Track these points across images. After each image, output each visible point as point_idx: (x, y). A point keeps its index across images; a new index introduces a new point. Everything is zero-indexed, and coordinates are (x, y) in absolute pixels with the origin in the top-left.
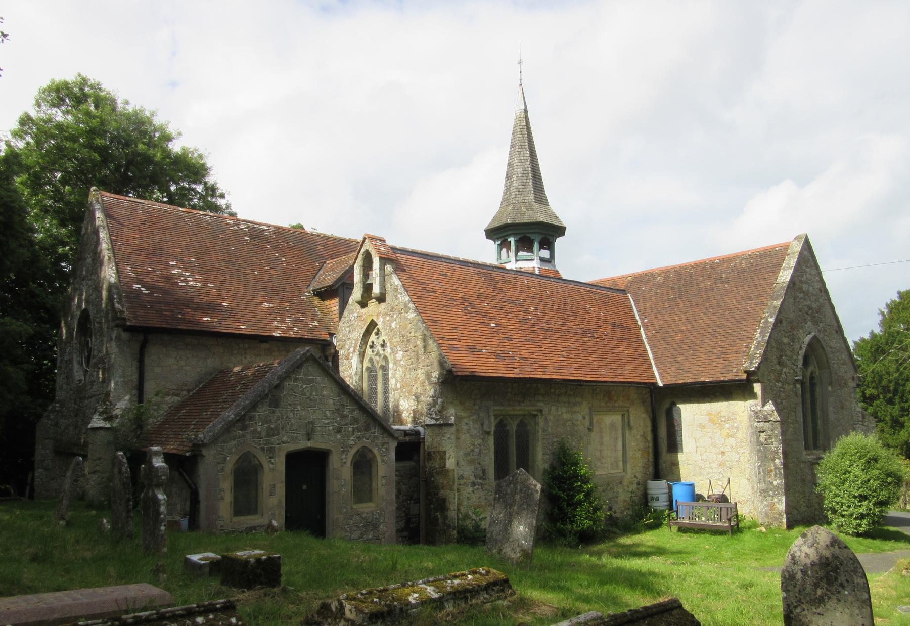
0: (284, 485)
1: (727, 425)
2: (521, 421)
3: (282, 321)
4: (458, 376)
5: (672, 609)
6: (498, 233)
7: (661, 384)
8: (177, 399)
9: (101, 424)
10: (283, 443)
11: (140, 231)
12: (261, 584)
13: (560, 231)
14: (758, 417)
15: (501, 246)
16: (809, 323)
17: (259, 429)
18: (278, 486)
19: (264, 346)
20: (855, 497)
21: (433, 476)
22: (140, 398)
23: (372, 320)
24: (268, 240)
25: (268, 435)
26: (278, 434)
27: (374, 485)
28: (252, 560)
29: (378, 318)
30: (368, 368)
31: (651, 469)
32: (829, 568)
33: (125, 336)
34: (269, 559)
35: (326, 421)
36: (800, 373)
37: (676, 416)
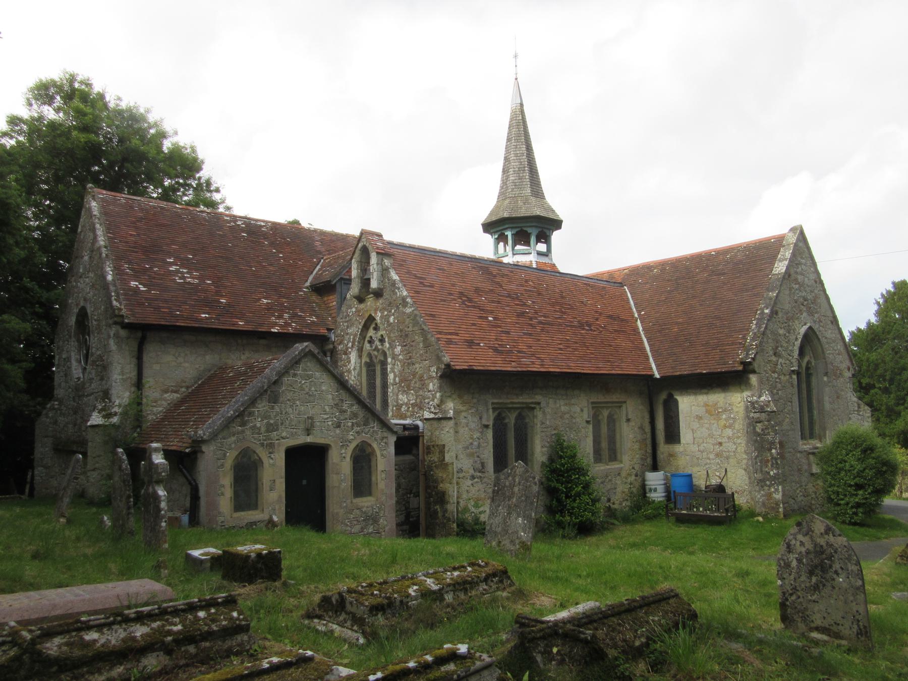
0: (284, 480)
1: (724, 416)
3: (280, 317)
4: (456, 370)
8: (176, 395)
10: (283, 438)
12: (262, 578)
13: (557, 224)
14: (754, 408)
15: (498, 241)
16: (805, 314)
17: (258, 425)
18: (277, 481)
19: (263, 342)
20: (851, 486)
23: (370, 315)
24: (265, 236)
25: (268, 431)
26: (277, 430)
27: (373, 479)
28: (253, 555)
30: (366, 363)
31: (649, 460)
32: (824, 556)
33: (123, 333)
34: (270, 553)
35: (326, 416)
36: (796, 364)
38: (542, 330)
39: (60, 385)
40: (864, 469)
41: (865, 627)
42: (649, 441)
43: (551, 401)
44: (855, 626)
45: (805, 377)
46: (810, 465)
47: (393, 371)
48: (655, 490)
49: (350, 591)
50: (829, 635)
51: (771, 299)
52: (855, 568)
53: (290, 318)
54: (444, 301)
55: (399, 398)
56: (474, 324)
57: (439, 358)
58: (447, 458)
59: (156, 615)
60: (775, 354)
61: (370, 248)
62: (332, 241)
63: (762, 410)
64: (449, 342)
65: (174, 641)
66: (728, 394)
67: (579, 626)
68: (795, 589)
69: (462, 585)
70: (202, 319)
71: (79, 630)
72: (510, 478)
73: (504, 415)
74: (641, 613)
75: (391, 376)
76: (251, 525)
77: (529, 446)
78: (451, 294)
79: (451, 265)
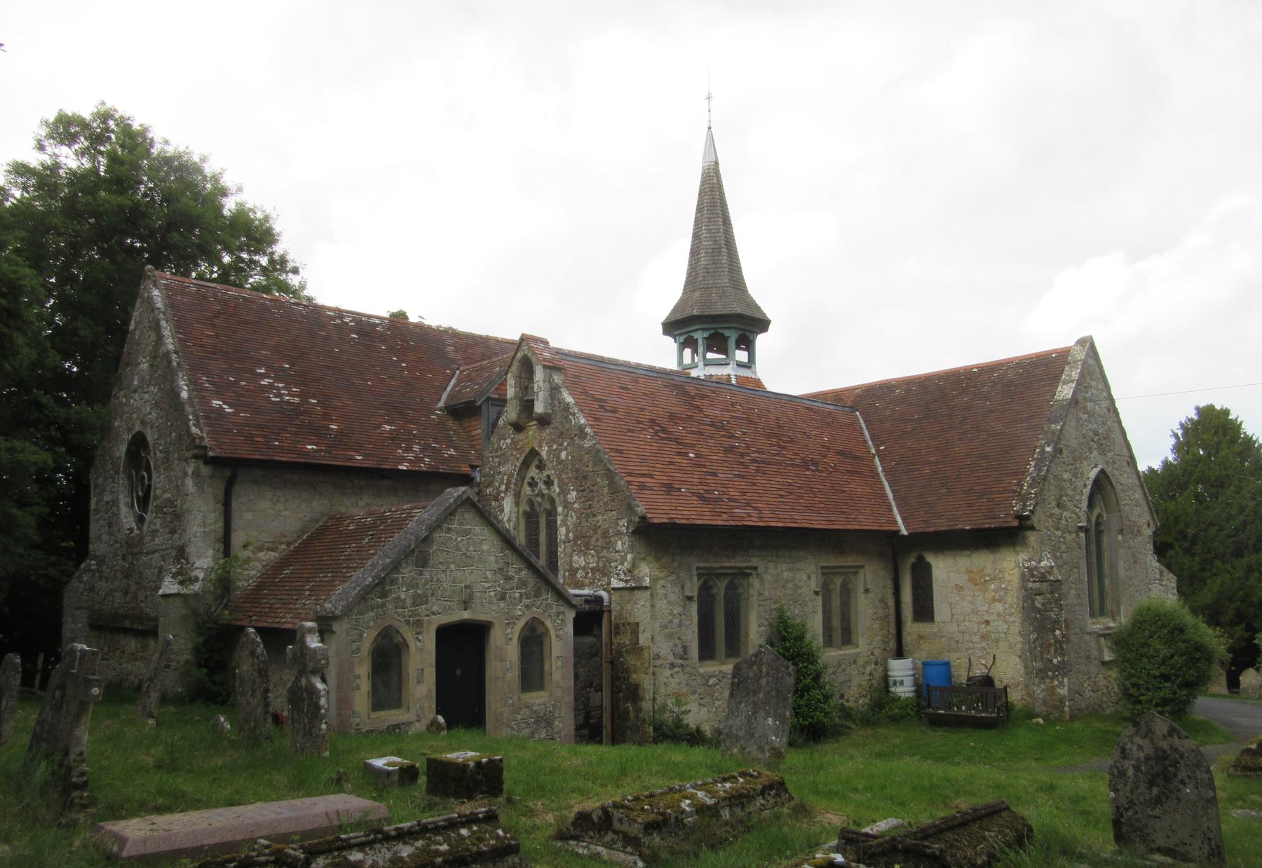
0: (434, 669)
1: (993, 586)
2: (731, 583)
3: (409, 449)
4: (654, 524)
5: (1000, 811)
6: (672, 326)
8: (273, 554)
10: (434, 613)
12: (482, 793)
14: (1033, 576)
15: (682, 346)
16: (1095, 453)
17: (403, 596)
18: (427, 671)
19: (386, 483)
20: (1155, 677)
21: (621, 656)
22: (227, 552)
23: (533, 449)
24: (381, 338)
25: (414, 604)
26: (426, 602)
27: (547, 667)
28: (472, 764)
29: (541, 446)
30: (525, 513)
31: (892, 644)
32: (1167, 763)
33: (205, 470)
34: (491, 761)
35: (487, 585)
36: (1084, 518)
38: (757, 471)
39: (99, 537)
40: (1172, 656)
41: (1218, 847)
42: (892, 619)
43: (771, 565)
44: (1207, 847)
45: (1094, 534)
46: (1100, 650)
48: (902, 683)
49: (616, 806)
50: (1175, 858)
51: (1053, 433)
52: (1205, 776)
53: (422, 451)
54: (632, 431)
55: (574, 560)
56: (671, 463)
57: (631, 509)
58: (643, 640)
59: (417, 833)
60: (1058, 505)
61: (534, 360)
62: (470, 346)
63: (1043, 579)
64: (643, 487)
65: (445, 862)
66: (998, 556)
67: (922, 839)
68: (1132, 802)
69: (737, 799)
70: (308, 452)
71: (341, 849)
73: (711, 583)
74: (975, 827)
75: (562, 531)
76: (394, 729)
77: (743, 623)
78: (640, 422)
79: (637, 382)
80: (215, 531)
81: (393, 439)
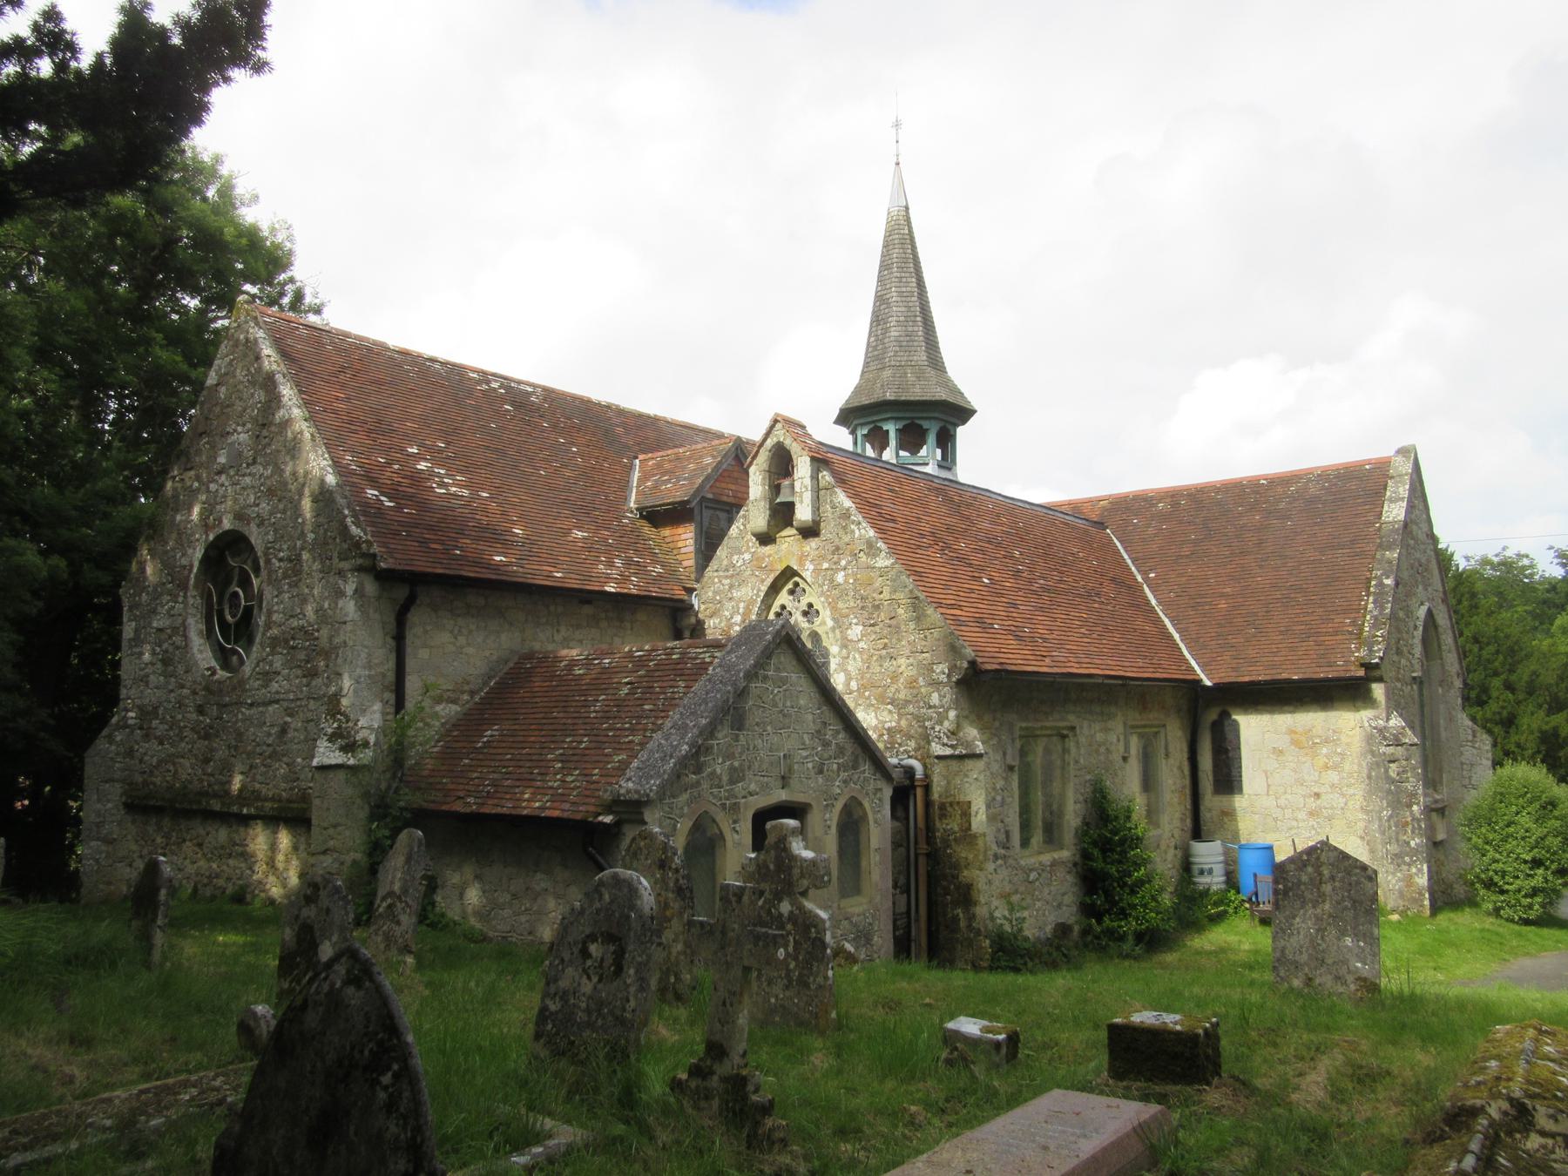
1: (1324, 751)
3: (610, 564)
7: (1208, 683)
8: (455, 708)
9: (336, 758)
11: (343, 386)
13: (960, 413)
14: (1385, 738)
19: (587, 610)
20: (1525, 862)
21: (949, 846)
22: (399, 704)
25: (732, 782)
26: (742, 779)
27: (864, 864)
29: (801, 564)
33: (371, 587)
35: (804, 753)
36: (1417, 666)
37: (1230, 736)
43: (1085, 724)
47: (842, 667)
61: (794, 448)
72: (1310, 869)
80: (384, 676)
81: (590, 550)
